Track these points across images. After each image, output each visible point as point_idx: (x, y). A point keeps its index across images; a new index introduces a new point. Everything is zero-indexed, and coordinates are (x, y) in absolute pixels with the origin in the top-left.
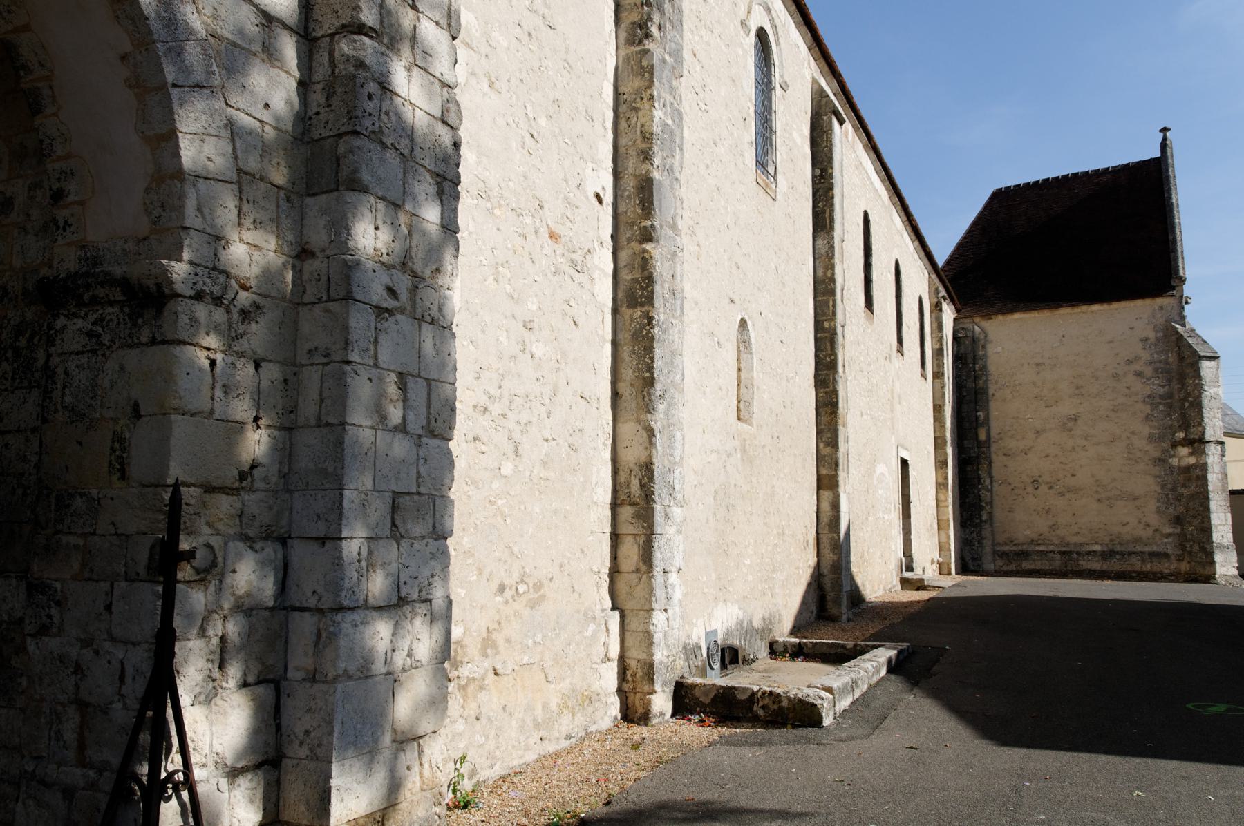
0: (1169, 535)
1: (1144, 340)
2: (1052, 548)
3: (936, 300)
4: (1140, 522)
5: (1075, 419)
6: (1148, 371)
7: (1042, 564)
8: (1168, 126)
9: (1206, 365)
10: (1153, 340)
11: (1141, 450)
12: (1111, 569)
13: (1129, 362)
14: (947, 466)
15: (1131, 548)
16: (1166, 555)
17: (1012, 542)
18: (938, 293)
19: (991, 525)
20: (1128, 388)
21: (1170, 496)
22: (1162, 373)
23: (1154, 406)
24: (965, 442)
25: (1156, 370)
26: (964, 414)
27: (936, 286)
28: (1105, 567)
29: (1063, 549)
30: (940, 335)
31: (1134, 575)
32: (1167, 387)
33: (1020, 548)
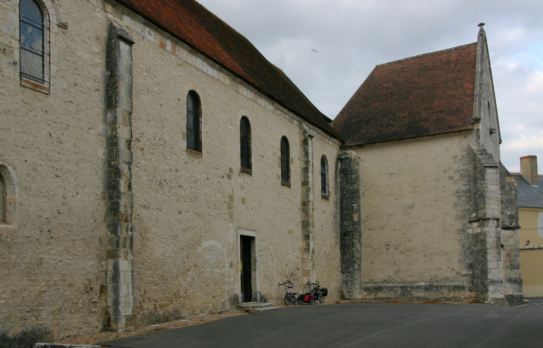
0: (466, 275)
2: (396, 284)
3: (303, 138)
5: (412, 207)
6: (456, 176)
7: (390, 294)
11: (450, 225)
13: (445, 171)
14: (309, 238)
15: (443, 284)
17: (373, 281)
19: (360, 272)
20: (444, 187)
21: (467, 252)
22: (464, 177)
23: (459, 197)
25: (461, 175)
26: (344, 206)
30: (306, 159)
32: (468, 186)
33: (377, 285)
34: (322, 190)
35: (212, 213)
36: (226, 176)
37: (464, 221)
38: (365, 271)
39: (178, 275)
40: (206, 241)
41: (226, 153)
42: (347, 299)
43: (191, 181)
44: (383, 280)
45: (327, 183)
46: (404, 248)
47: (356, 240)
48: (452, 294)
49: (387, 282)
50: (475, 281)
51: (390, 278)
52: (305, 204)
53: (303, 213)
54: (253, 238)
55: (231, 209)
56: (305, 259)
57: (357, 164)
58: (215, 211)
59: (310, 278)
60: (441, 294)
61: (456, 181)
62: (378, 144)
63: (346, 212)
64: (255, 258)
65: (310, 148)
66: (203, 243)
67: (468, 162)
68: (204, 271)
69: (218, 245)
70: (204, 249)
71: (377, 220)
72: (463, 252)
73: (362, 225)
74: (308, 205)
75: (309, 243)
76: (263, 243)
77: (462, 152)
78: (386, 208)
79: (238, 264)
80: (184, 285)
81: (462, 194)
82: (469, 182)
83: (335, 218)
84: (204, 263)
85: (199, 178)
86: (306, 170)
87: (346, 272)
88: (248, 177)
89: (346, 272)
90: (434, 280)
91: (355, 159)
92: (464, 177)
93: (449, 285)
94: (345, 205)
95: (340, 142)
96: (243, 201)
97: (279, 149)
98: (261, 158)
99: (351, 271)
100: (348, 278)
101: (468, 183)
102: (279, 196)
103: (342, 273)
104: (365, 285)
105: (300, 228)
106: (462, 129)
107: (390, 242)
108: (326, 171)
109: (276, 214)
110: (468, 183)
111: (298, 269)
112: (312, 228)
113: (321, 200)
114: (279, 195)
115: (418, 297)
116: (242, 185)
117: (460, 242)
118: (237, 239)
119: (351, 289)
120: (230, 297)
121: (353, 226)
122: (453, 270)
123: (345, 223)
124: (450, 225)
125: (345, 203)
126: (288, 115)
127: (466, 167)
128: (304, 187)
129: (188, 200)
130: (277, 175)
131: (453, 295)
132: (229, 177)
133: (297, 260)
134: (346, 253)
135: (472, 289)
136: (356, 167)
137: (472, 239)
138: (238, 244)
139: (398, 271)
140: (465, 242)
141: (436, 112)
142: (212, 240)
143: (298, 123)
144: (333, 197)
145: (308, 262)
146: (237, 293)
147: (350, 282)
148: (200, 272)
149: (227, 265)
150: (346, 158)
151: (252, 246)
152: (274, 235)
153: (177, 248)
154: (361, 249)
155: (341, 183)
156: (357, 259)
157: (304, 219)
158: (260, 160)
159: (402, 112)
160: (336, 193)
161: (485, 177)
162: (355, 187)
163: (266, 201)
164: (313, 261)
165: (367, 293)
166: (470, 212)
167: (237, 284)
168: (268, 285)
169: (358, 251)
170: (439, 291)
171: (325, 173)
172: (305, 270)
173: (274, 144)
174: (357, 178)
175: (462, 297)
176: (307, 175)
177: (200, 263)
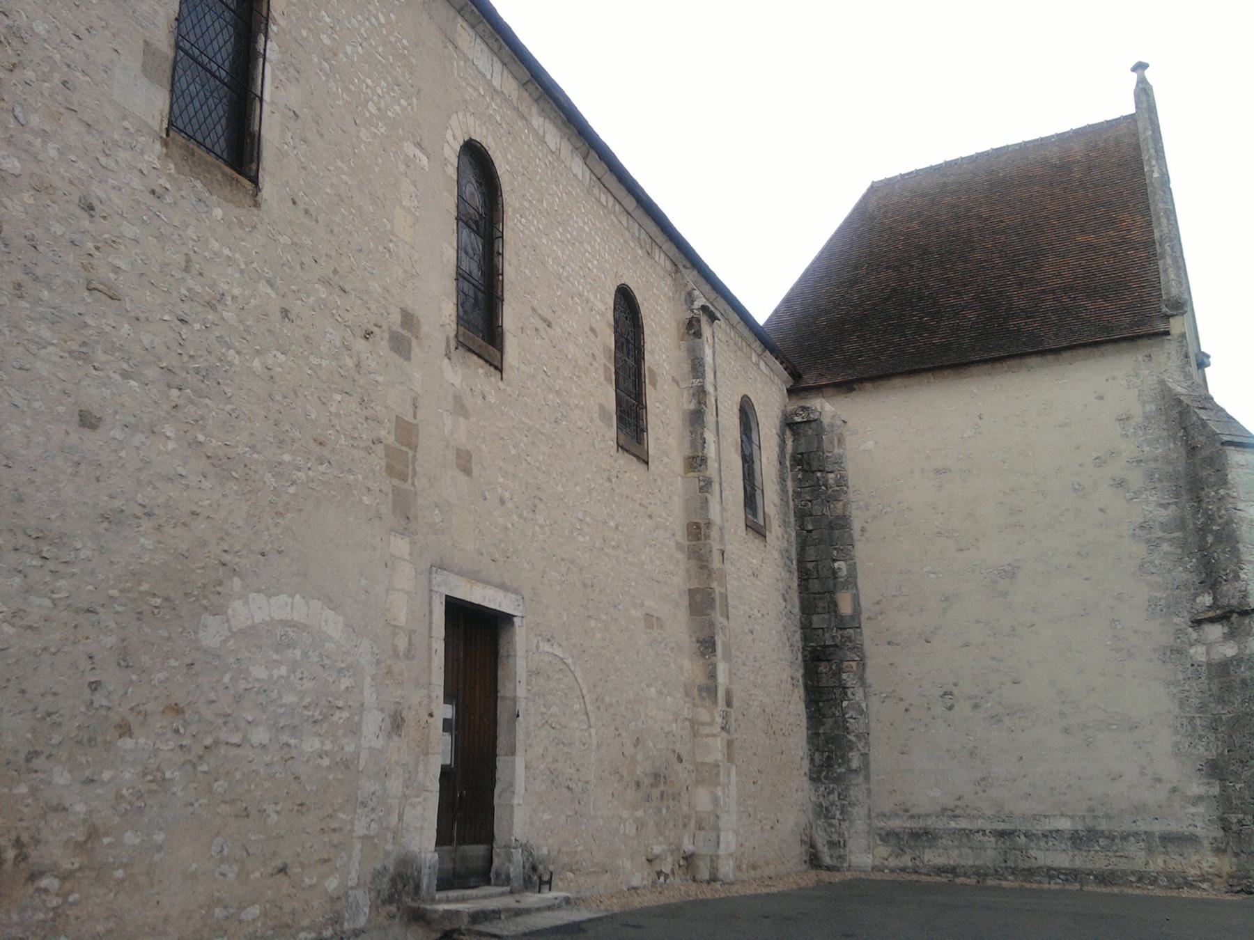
0: (1200, 798)
1: (1124, 419)
2: (980, 824)
3: (689, 315)
4: (1143, 774)
5: (1011, 573)
6: (1136, 478)
7: (961, 855)
8: (1144, 60)
9: (1236, 457)
10: (1138, 419)
11: (1136, 632)
12: (1090, 866)
13: (1100, 462)
14: (714, 650)
15: (1127, 826)
16: (1192, 840)
17: (907, 811)
18: (692, 302)
19: (867, 778)
20: (1102, 510)
21: (1198, 722)
22: (1160, 480)
23: (1153, 544)
24: (815, 618)
25: (1150, 476)
26: (810, 566)
27: (689, 289)
28: (1078, 863)
29: (1002, 826)
30: (696, 382)
31: (1133, 879)
32: (1173, 507)
33: (921, 823)
34: (745, 505)
35: (302, 475)
36: (386, 335)
37: (1176, 620)
38: (883, 777)
39: (36, 754)
40: (257, 599)
41: (391, 245)
42: (829, 868)
43: (184, 291)
44: (939, 808)
45: (758, 483)
46: (1000, 703)
47: (851, 675)
48: (1158, 863)
49: (950, 813)
50: (1234, 818)
51: (959, 803)
52: (697, 531)
53: (693, 562)
54: (507, 619)
55: (403, 477)
56: (703, 724)
57: (839, 441)
58: (322, 468)
59: (720, 794)
60: (1125, 860)
61: (1134, 493)
62: (897, 382)
63: (815, 585)
64: (514, 700)
65: (708, 352)
66: (237, 604)
67: (1165, 433)
68: (235, 739)
69: (332, 625)
70: (241, 631)
71: (911, 615)
72: (1185, 722)
73: (867, 630)
74: (707, 537)
75: (714, 667)
76: (546, 647)
77: (1144, 403)
78: (932, 576)
79: (431, 720)
80: (80, 808)
81: (1161, 534)
82: (1177, 496)
83: (785, 600)
84: (238, 699)
85: (236, 292)
86: (696, 418)
87: (826, 777)
88: (486, 374)
89: (826, 777)
90: (1101, 814)
91: (832, 425)
92: (1160, 480)
93: (1148, 829)
94: (813, 564)
95: (790, 374)
96: (465, 462)
97: (608, 323)
98: (542, 326)
99: (839, 775)
100: (831, 797)
101: (1173, 500)
102: (607, 484)
103: (811, 779)
104: (882, 824)
105: (683, 615)
106: (1138, 331)
107: (955, 685)
108: (755, 448)
109: (597, 545)
110: (1173, 500)
111: (680, 760)
112: (722, 615)
113: (744, 534)
114: (609, 480)
115: (1050, 869)
116: (458, 399)
117: (1171, 687)
118: (431, 613)
119: (841, 835)
120: (378, 866)
121: (840, 632)
122: (1159, 780)
123: (815, 619)
124: (1136, 632)
125: (813, 559)
126: (636, 226)
127: (1160, 451)
128: (692, 474)
129: (151, 373)
130: (601, 407)
131: (1162, 865)
132: (400, 345)
133: (674, 726)
134: (824, 716)
135: (1223, 846)
136: (836, 451)
137: (1210, 678)
138: (434, 633)
139: (983, 779)
140: (1187, 687)
141: (1053, 291)
142: (292, 596)
143: (669, 266)
144: (780, 535)
145: (714, 735)
146: (415, 848)
147: (838, 813)
148: (208, 741)
149: (373, 722)
150: (809, 422)
151: (502, 652)
152: (593, 623)
153: (48, 603)
154: (867, 705)
155: (797, 495)
156: (857, 736)
157: (695, 584)
158: (537, 330)
159: (955, 293)
160: (785, 523)
161: (1229, 477)
162: (837, 511)
163: (560, 489)
164: (728, 732)
165: (890, 849)
166: (1192, 591)
167: (419, 808)
168: (563, 817)
169: (861, 712)
170: (1117, 851)
171: (751, 454)
172: (703, 764)
173: (592, 299)
174: (842, 482)
175: (1193, 872)
176: (702, 434)
177: (212, 696)
